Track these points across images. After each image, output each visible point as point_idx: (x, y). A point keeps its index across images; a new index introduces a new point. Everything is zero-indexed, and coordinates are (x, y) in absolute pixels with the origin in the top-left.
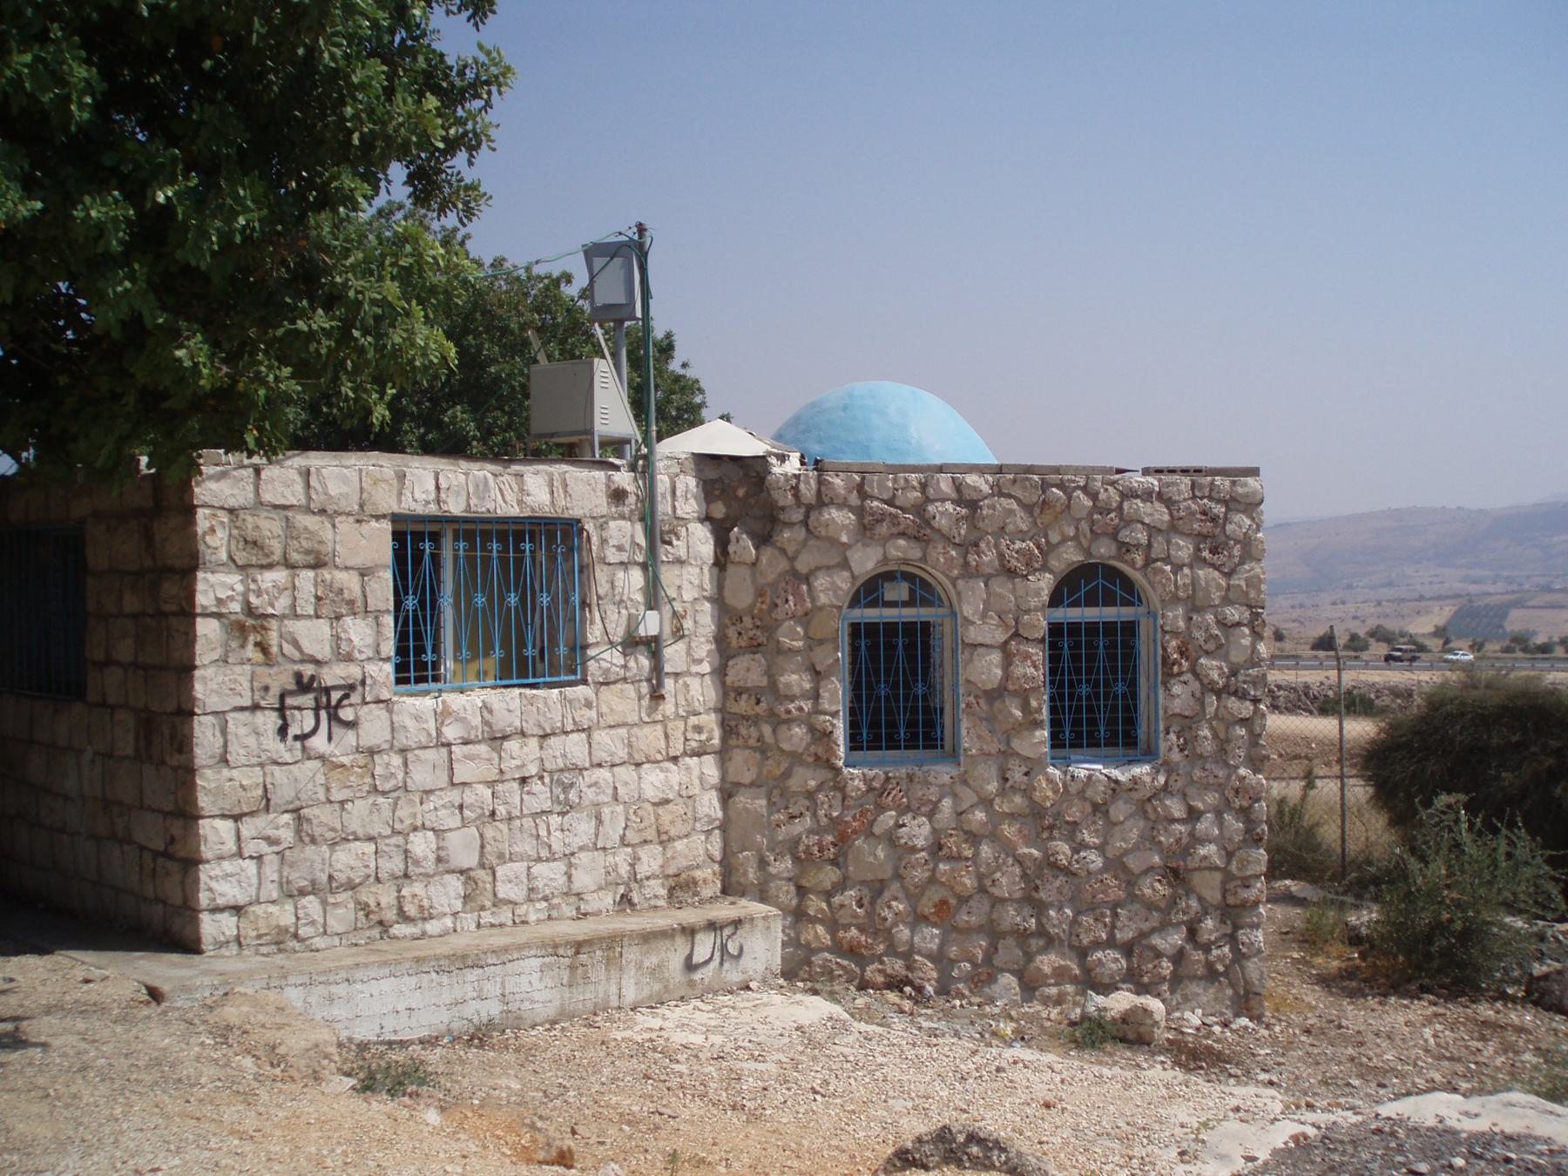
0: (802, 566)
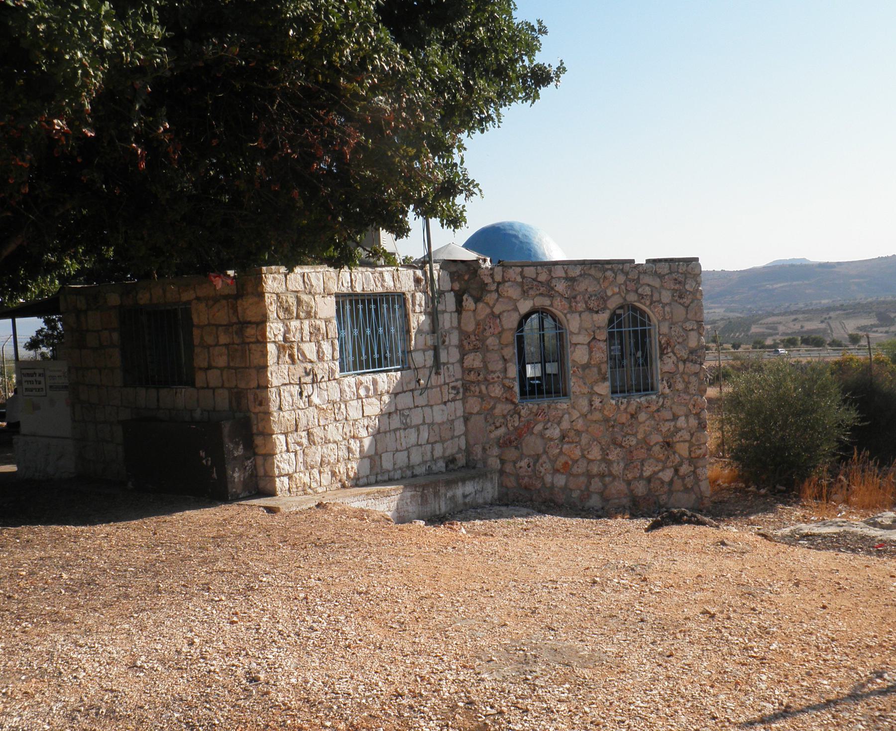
0: (497, 311)
